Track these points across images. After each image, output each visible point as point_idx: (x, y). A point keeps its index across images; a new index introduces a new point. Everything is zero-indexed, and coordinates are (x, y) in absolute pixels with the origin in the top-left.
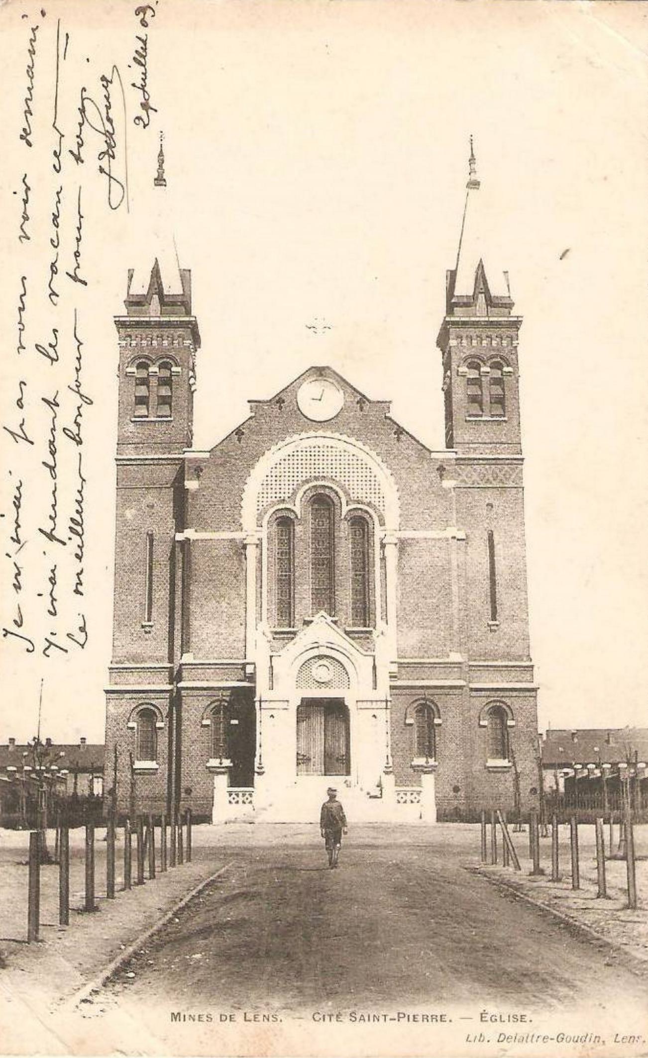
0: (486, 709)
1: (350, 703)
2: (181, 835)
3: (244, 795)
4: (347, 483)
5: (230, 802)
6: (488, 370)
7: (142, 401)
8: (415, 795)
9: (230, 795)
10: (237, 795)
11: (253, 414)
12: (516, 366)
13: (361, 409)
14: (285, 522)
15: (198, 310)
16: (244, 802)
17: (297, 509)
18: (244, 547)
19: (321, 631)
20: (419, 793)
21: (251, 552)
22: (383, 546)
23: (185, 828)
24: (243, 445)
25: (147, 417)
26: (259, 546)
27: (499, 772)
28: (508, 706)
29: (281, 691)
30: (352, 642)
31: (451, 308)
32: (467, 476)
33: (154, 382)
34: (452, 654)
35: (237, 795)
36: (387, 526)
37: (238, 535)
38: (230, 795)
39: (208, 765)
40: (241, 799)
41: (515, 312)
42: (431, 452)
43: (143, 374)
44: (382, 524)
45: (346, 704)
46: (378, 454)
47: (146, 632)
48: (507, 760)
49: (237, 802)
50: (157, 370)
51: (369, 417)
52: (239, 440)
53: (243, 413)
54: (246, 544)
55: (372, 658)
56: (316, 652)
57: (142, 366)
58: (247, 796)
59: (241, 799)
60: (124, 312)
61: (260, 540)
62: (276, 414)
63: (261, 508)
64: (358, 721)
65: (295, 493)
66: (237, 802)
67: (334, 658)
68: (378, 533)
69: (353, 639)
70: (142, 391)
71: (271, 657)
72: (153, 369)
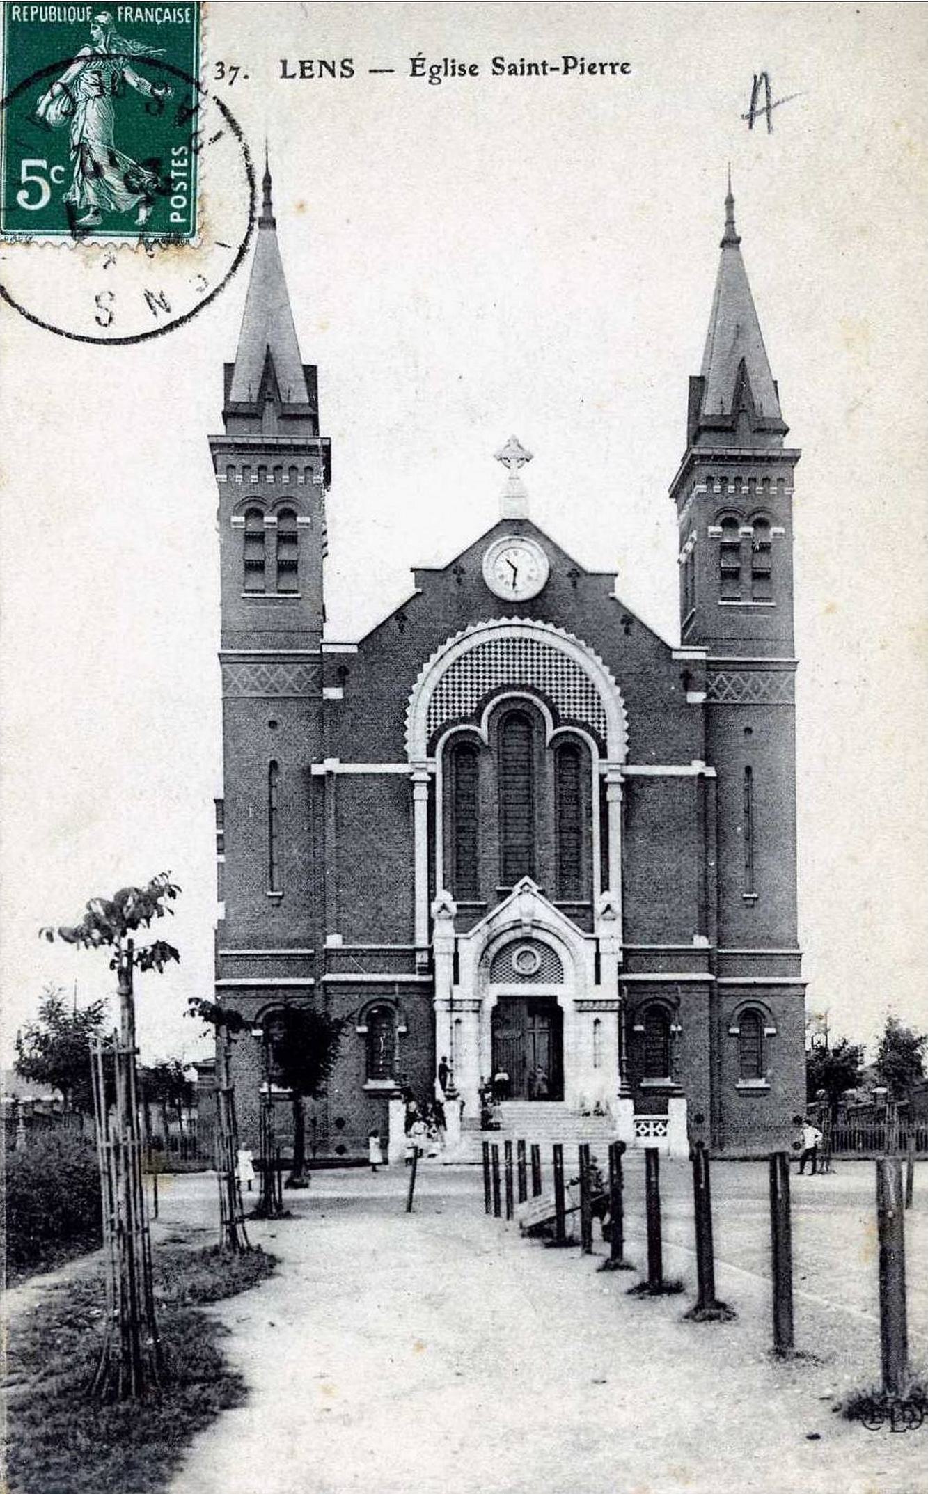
0: (738, 1012)
1: (566, 1003)
2: (900, 1174)
3: (655, 1125)
4: (554, 694)
5: (665, 1134)
6: (275, 519)
7: (254, 567)
8: (660, 1125)
9: (638, 1125)
10: (647, 1125)
11: (420, 590)
12: (788, 525)
13: (575, 585)
14: (462, 752)
15: (326, 427)
16: (656, 1134)
17: (483, 731)
18: (412, 785)
19: (528, 905)
20: (665, 1123)
21: (421, 793)
22: (604, 787)
23: (904, 1167)
24: (400, 640)
25: (263, 591)
26: (431, 785)
27: (752, 1096)
28: (767, 1008)
29: (465, 991)
30: (567, 919)
31: (693, 438)
32: (717, 687)
33: (272, 540)
34: (696, 937)
35: (647, 1125)
36: (611, 759)
37: (402, 768)
38: (638, 1125)
39: (366, 1087)
40: (651, 1129)
41: (789, 442)
42: (671, 650)
43: (253, 526)
44: (603, 754)
45: (560, 1003)
46: (597, 654)
47: (747, 906)
48: (764, 1080)
49: (647, 1134)
50: (275, 519)
51: (571, 595)
52: (401, 628)
53: (406, 588)
54: (413, 782)
55: (594, 943)
56: (518, 934)
57: (730, 524)
58: (660, 1125)
59: (651, 1129)
60: (220, 429)
61: (433, 775)
62: (452, 593)
63: (432, 729)
64: (576, 1030)
65: (480, 710)
66: (647, 1134)
67: (543, 943)
68: (598, 767)
69: (568, 916)
70: (254, 553)
71: (456, 940)
72: (270, 519)
